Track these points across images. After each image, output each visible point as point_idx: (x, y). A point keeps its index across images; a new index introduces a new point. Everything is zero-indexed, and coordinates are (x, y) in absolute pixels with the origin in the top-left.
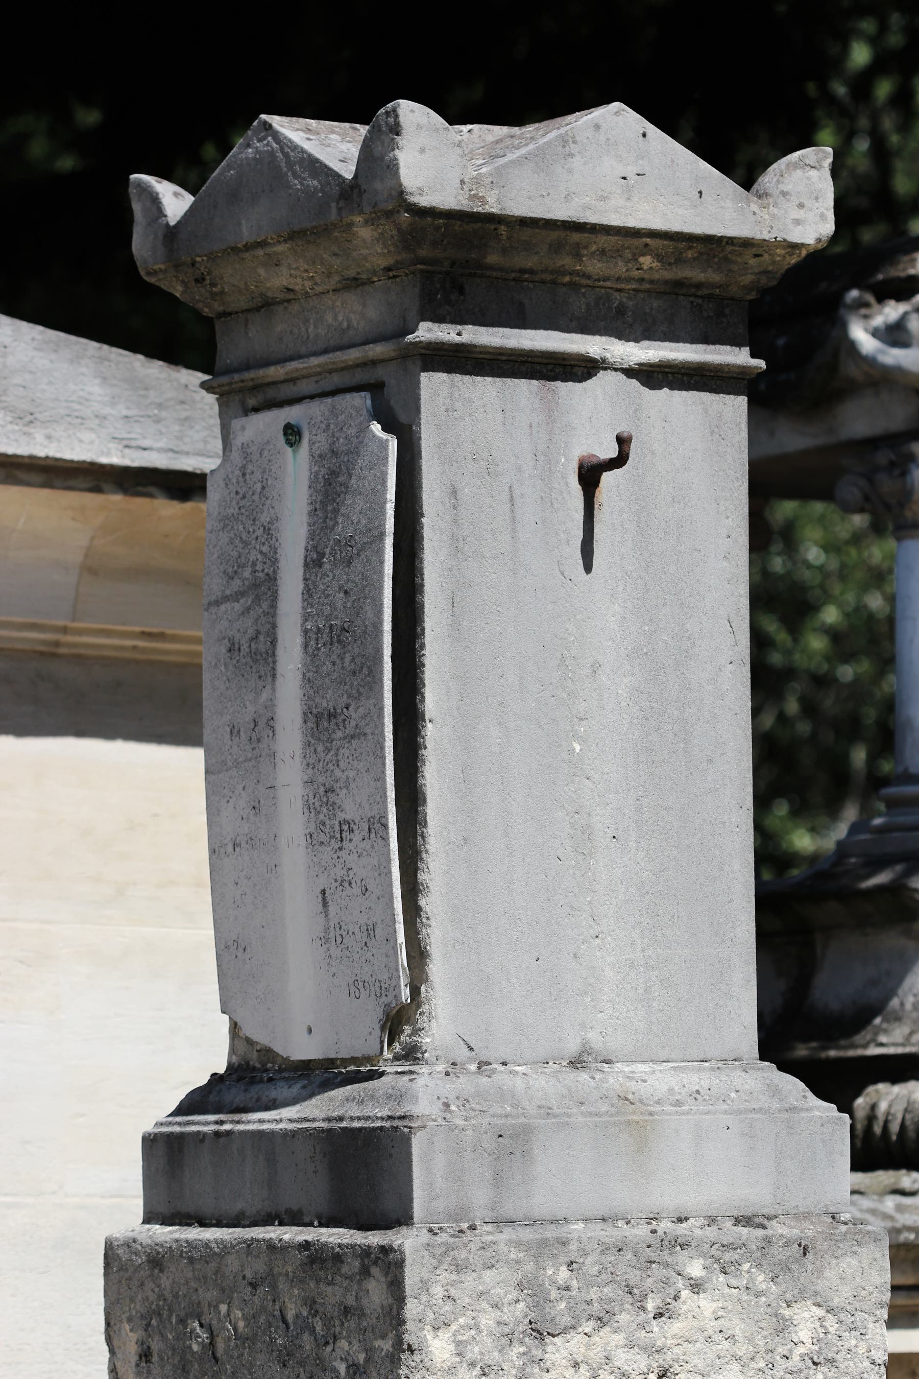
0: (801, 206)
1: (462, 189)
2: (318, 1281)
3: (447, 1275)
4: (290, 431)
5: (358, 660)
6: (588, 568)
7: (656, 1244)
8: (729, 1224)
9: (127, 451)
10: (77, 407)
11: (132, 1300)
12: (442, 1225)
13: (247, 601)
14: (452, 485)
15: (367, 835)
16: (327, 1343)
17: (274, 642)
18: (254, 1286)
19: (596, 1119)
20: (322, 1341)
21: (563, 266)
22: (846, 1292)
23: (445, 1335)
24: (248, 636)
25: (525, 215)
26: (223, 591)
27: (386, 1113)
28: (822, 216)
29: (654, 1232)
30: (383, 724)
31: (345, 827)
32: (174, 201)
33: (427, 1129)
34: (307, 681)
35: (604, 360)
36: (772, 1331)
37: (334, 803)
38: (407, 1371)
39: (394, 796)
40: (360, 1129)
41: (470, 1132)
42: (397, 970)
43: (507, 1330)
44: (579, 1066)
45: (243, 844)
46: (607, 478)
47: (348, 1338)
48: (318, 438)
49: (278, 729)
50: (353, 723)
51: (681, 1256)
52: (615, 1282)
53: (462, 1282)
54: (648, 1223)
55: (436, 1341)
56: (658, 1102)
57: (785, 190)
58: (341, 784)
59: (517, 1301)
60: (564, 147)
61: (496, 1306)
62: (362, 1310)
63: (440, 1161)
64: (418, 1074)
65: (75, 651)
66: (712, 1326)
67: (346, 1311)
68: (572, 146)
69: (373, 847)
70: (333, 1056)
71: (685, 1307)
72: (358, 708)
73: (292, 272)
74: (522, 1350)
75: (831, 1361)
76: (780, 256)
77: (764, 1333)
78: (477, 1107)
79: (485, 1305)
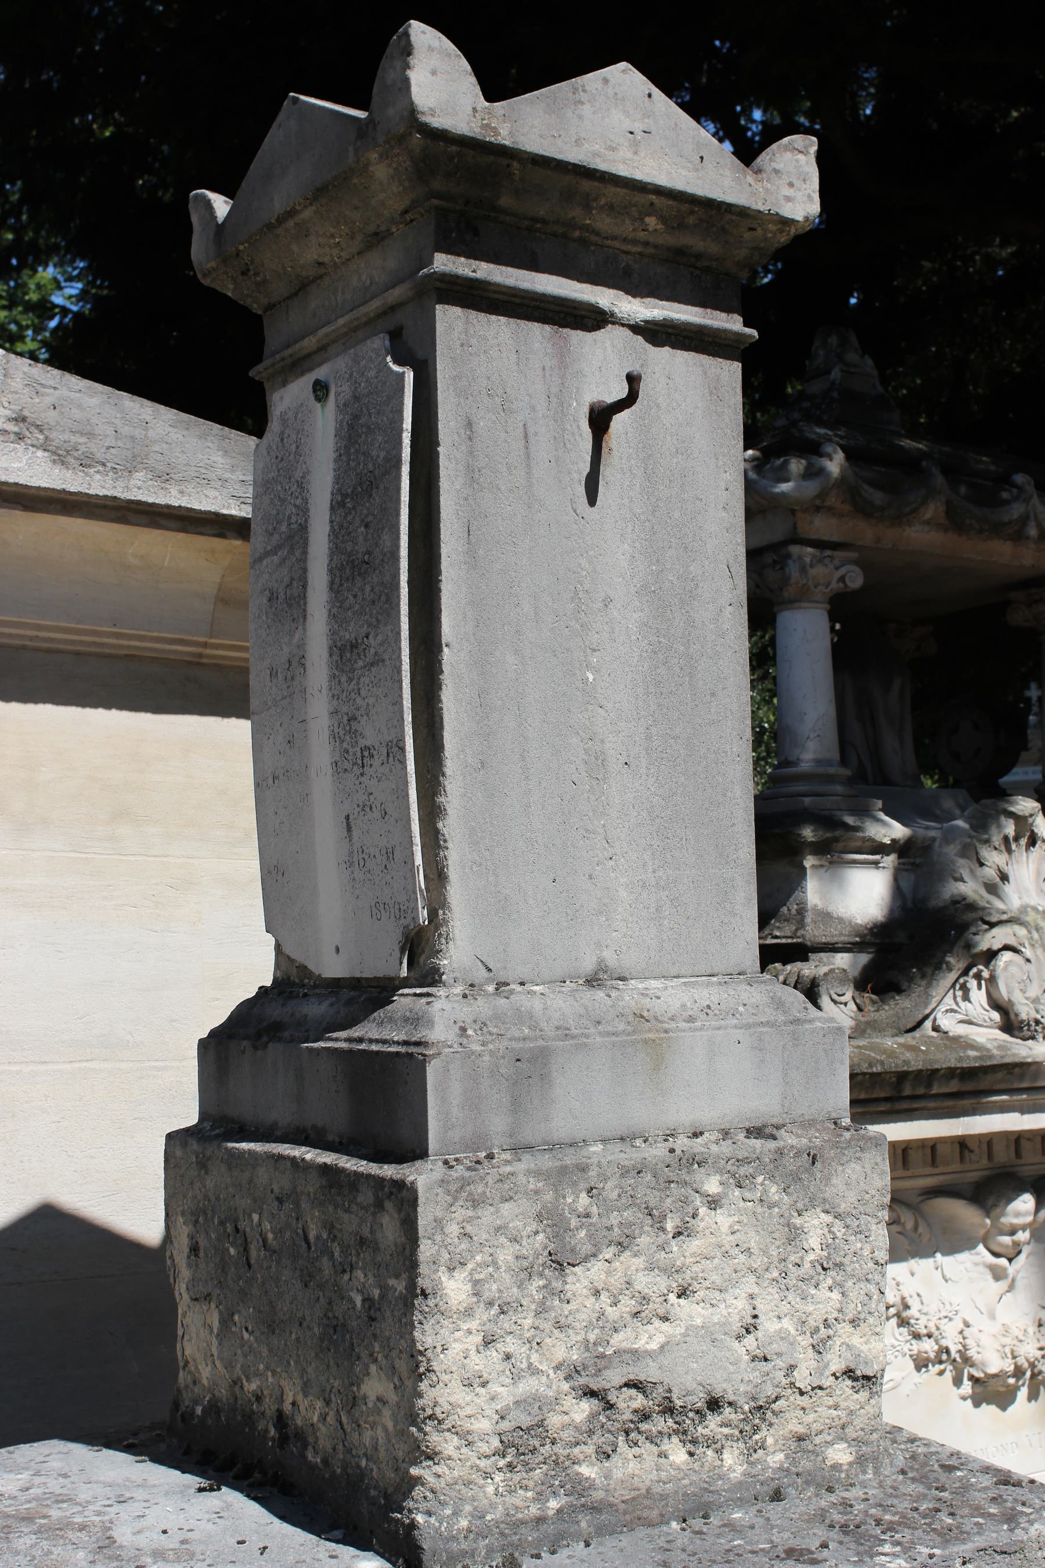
0: (791, 185)
1: (475, 116)
2: (336, 1207)
3: (463, 1211)
4: (318, 387)
5: (377, 590)
6: (592, 496)
7: (675, 1164)
8: (741, 1136)
9: (243, 506)
10: (204, 471)
11: (185, 1196)
12: (458, 1156)
13: (283, 553)
14: (467, 417)
15: (385, 759)
16: (344, 1271)
17: (305, 587)
18: (280, 1200)
19: (614, 1038)
20: (339, 1268)
21: (574, 218)
22: (852, 1197)
23: (461, 1275)
24: (284, 584)
25: (537, 152)
26: (265, 548)
27: (402, 1037)
28: (809, 196)
29: (672, 1151)
30: (400, 649)
31: (366, 754)
32: (221, 205)
33: (442, 1057)
34: (332, 616)
35: (612, 314)
36: (785, 1240)
37: (356, 731)
38: (420, 1317)
39: (410, 719)
40: (378, 1053)
41: (486, 1058)
42: (415, 893)
43: (525, 1264)
44: (595, 984)
45: (281, 776)
46: (619, 421)
47: (364, 1269)
48: (343, 388)
49: (308, 665)
50: (372, 651)
51: (699, 1173)
52: (635, 1205)
53: (479, 1218)
54: (666, 1140)
55: (452, 1282)
56: (672, 1019)
57: (777, 168)
58: (362, 711)
59: (537, 1233)
60: (574, 93)
61: (515, 1240)
62: (377, 1243)
63: (456, 1090)
64: (435, 996)
65: (214, 661)
66: (728, 1240)
67: (362, 1242)
68: (582, 94)
69: (391, 771)
70: (358, 975)
71: (702, 1225)
72: (377, 635)
73: (321, 240)
74: (541, 1283)
75: (839, 1265)
76: (771, 232)
77: (778, 1243)
78: (495, 1030)
79: (503, 1240)
